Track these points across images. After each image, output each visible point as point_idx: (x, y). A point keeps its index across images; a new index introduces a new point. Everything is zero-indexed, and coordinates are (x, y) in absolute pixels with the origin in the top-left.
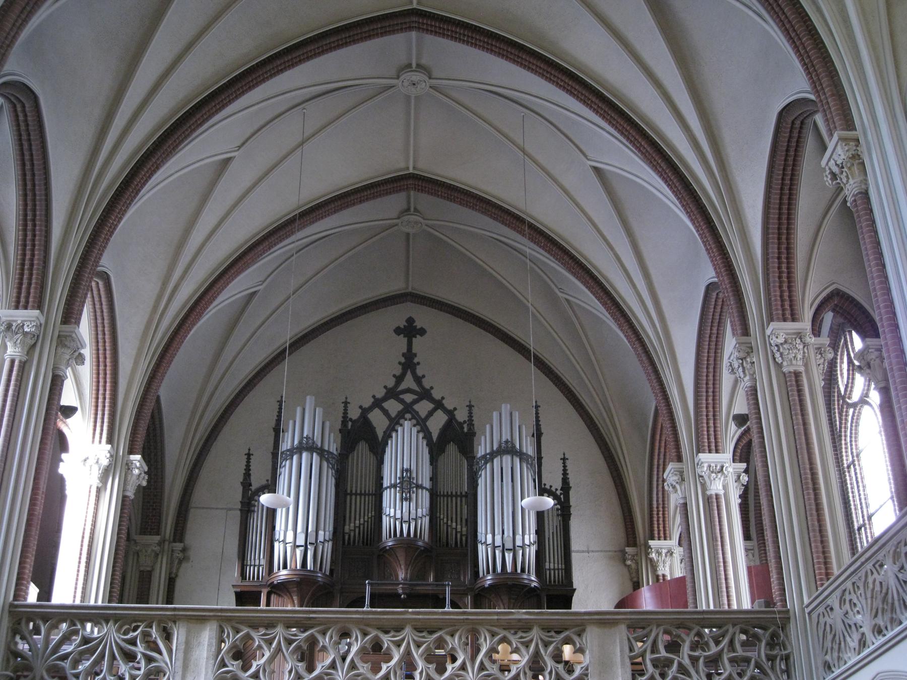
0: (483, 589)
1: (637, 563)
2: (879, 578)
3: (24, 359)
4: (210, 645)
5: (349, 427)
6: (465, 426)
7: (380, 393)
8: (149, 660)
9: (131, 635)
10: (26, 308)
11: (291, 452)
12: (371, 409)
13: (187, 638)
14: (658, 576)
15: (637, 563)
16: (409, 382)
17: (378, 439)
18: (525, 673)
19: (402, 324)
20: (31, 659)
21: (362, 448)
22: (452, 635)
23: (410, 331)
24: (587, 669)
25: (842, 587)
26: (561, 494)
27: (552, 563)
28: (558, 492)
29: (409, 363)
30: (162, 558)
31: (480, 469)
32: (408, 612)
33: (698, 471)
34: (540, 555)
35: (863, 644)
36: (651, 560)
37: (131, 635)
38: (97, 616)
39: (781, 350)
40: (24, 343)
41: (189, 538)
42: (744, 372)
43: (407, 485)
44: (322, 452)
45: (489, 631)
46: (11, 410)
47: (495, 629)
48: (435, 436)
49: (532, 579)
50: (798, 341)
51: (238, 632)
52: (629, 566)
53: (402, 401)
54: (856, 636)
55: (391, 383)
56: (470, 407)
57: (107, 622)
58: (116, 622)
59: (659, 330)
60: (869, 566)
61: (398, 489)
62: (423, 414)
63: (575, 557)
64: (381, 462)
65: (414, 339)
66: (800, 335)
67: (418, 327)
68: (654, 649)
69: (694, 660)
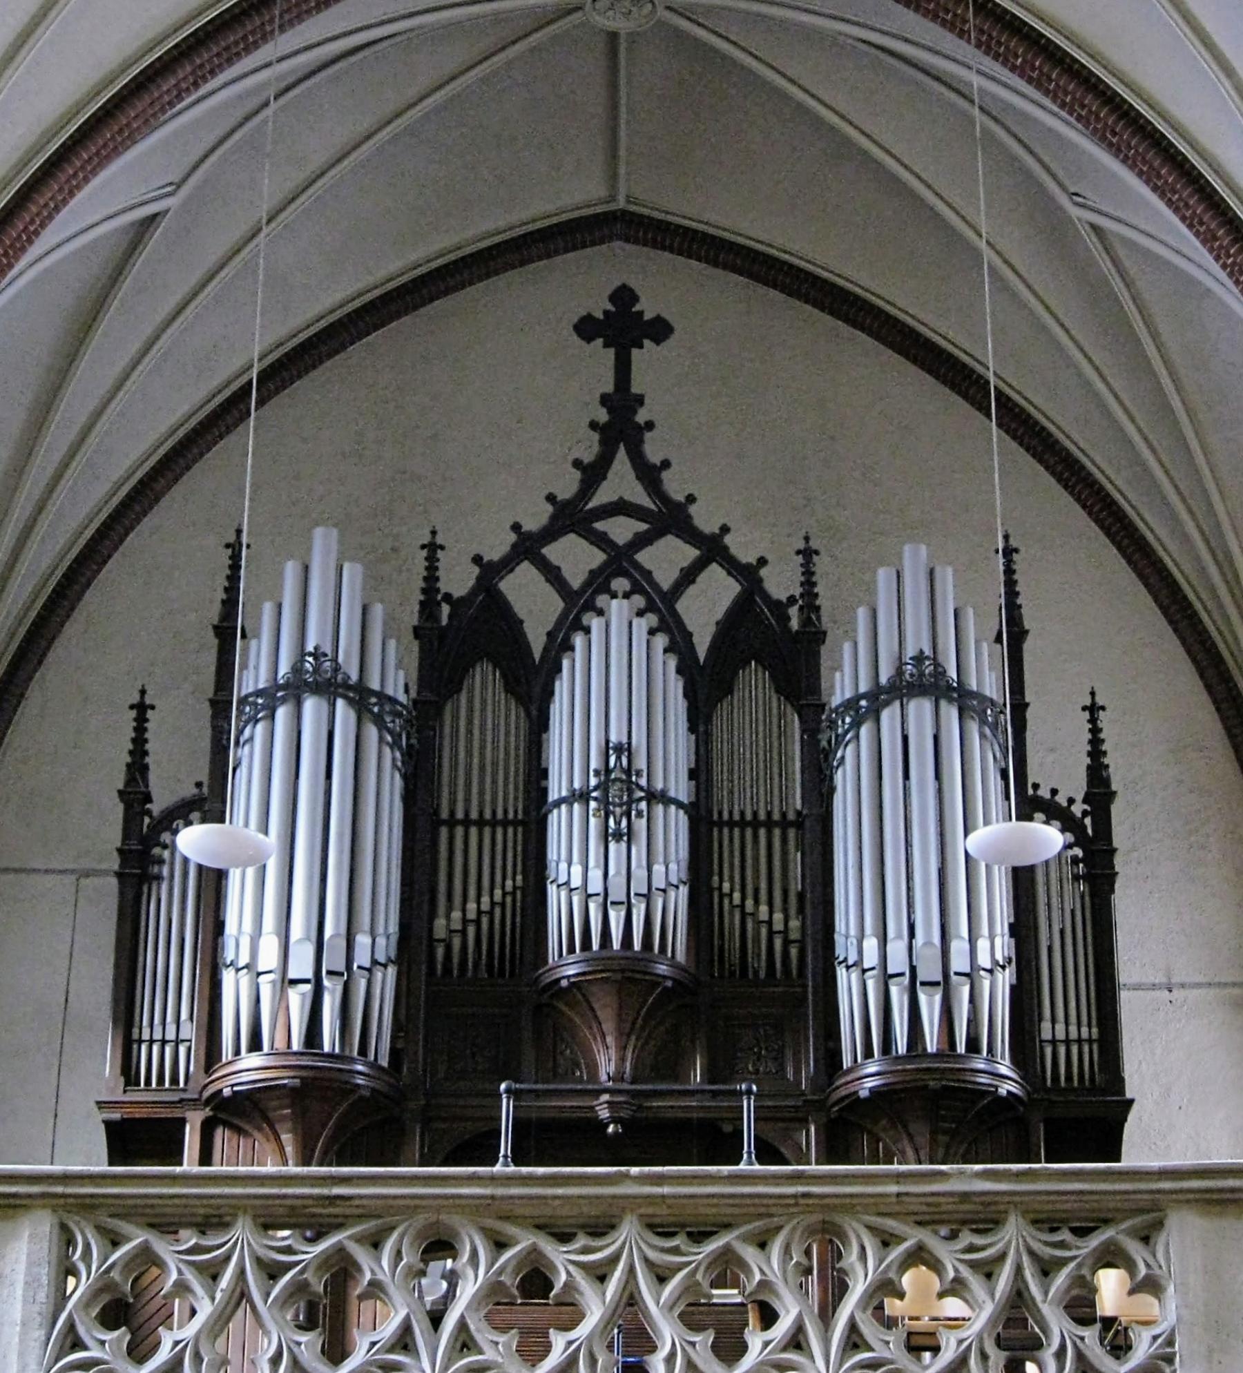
0: (854, 1102)
6: (793, 611)
7: (536, 517)
11: (270, 698)
12: (507, 564)
18: (984, 1357)
19: (600, 306)
24: (1170, 1342)
26: (1085, 813)
28: (1077, 809)
32: (627, 1176)
44: (360, 696)
45: (870, 1228)
47: (891, 1224)
48: (702, 644)
53: (601, 540)
55: (567, 485)
56: (808, 554)
61: (593, 804)
62: (666, 578)
63: (1128, 1003)
64: (539, 725)
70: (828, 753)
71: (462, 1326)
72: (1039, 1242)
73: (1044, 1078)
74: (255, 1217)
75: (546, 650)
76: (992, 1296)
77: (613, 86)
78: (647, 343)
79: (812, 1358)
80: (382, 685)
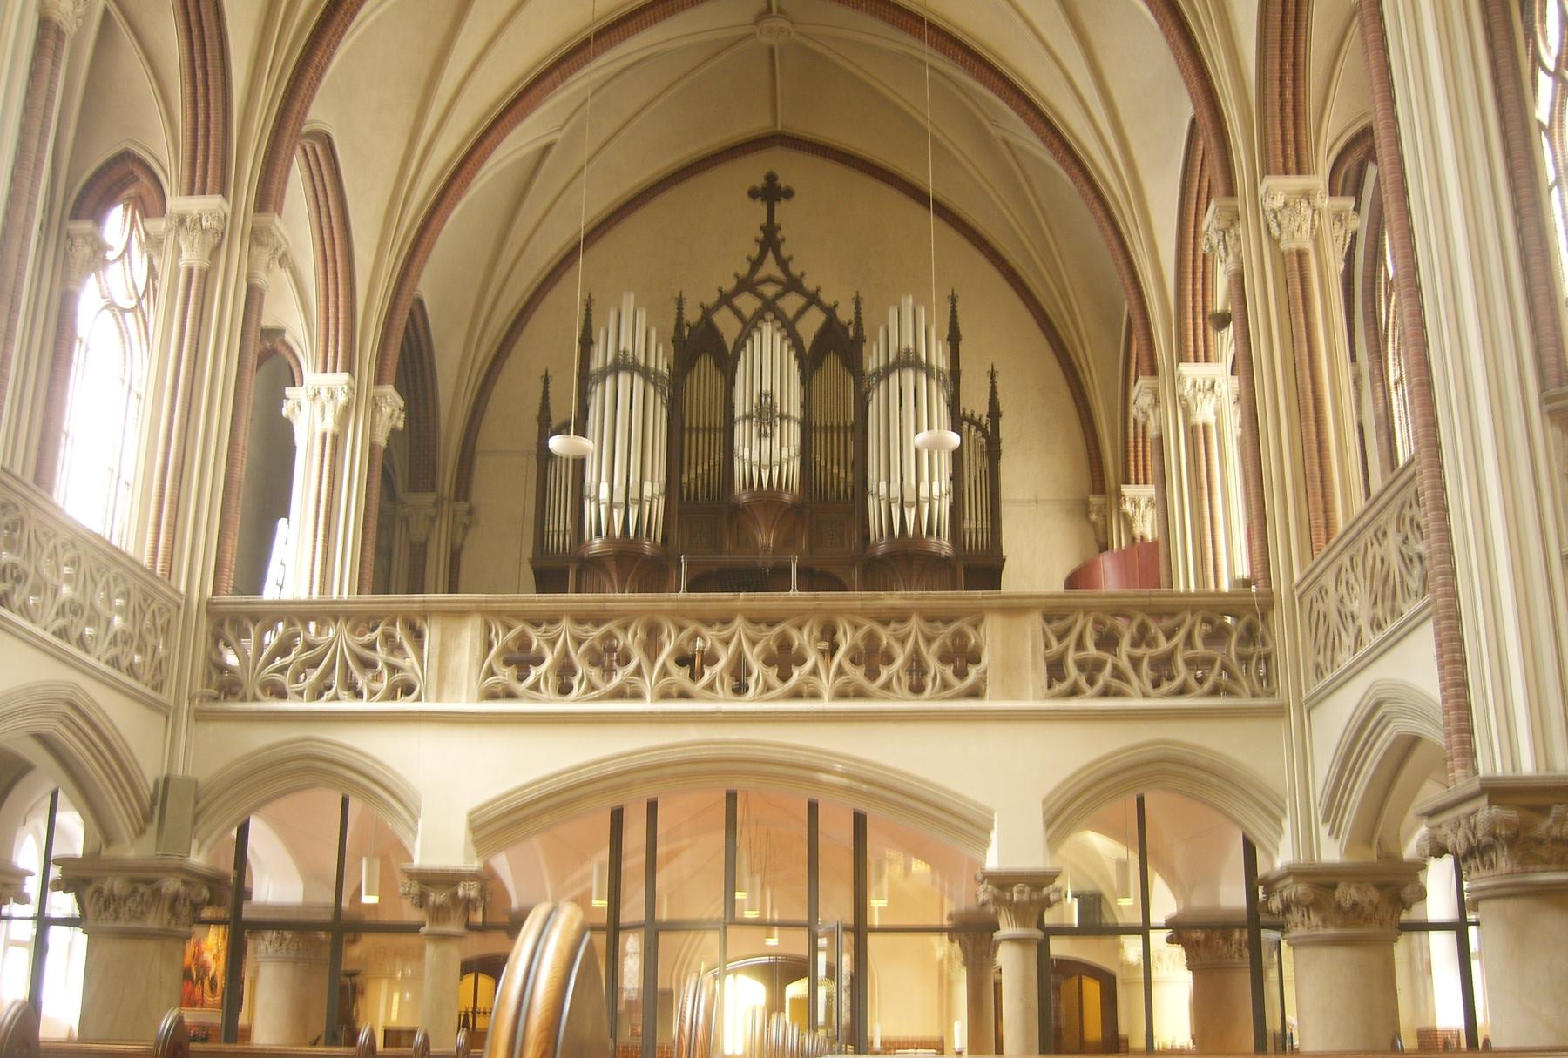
0: (874, 559)
1: (1105, 517)
2: (1379, 552)
3: (206, 265)
4: (472, 647)
5: (686, 334)
7: (729, 285)
8: (393, 669)
9: (369, 637)
10: (203, 192)
11: (603, 374)
12: (717, 307)
13: (442, 640)
14: (1134, 539)
15: (1105, 517)
16: (770, 267)
17: (726, 350)
18: (899, 679)
19: (759, 182)
20: (239, 672)
21: (705, 364)
22: (800, 628)
23: (771, 192)
24: (985, 672)
25: (1338, 562)
27: (974, 521)
29: (770, 240)
30: (441, 522)
31: (870, 390)
33: (1179, 389)
34: (956, 511)
35: (1358, 640)
36: (1125, 515)
37: (369, 637)
38: (325, 613)
39: (1279, 217)
40: (203, 242)
41: (476, 494)
42: (1226, 248)
43: (766, 415)
44: (646, 373)
46: (192, 338)
47: (858, 620)
48: (807, 344)
49: (944, 545)
50: (1304, 204)
51: (510, 629)
52: (1094, 525)
53: (761, 296)
54: (1352, 630)
55: (744, 269)
57: (336, 621)
58: (347, 620)
59: (1127, 185)
60: (1369, 533)
61: (754, 419)
62: (790, 313)
63: (1006, 511)
64: (730, 384)
65: (776, 203)
66: (1307, 196)
67: (783, 186)
68: (1080, 645)
69: (1135, 662)
70: (867, 393)
71: (664, 665)
72: (927, 629)
73: (965, 547)
74: (572, 616)
75: (734, 348)
76: (904, 652)
77: (773, 73)
78: (782, 198)
79: (821, 679)
80: (111, 537)
